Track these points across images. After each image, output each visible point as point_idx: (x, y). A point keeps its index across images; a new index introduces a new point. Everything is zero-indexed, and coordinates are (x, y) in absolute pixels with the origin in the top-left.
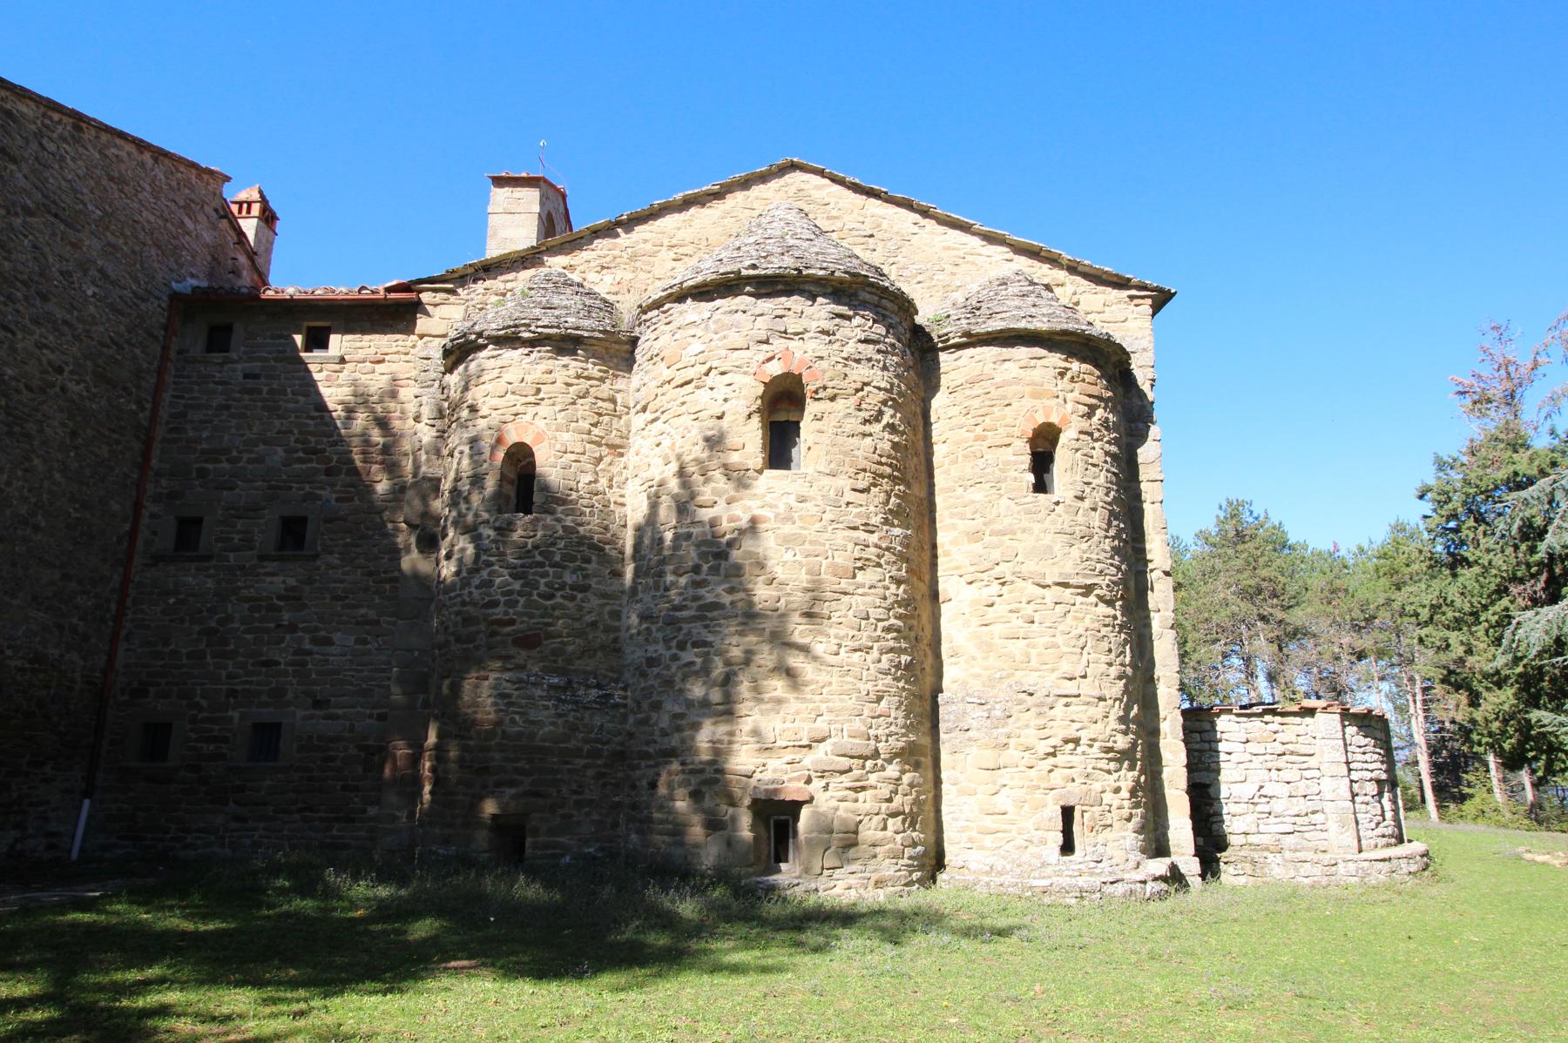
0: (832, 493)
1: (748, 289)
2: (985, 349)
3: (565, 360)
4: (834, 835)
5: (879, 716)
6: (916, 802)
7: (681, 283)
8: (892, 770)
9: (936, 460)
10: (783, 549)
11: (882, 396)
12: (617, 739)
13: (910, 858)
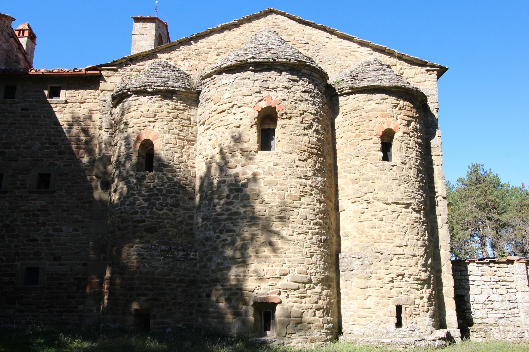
0: (290, 161)
1: (251, 68)
2: (360, 95)
3: (168, 101)
4: (291, 318)
5: (312, 264)
6: (329, 303)
7: (220, 66)
8: (318, 289)
9: (338, 146)
10: (267, 187)
11: (312, 117)
12: (192, 274)
13: (326, 329)
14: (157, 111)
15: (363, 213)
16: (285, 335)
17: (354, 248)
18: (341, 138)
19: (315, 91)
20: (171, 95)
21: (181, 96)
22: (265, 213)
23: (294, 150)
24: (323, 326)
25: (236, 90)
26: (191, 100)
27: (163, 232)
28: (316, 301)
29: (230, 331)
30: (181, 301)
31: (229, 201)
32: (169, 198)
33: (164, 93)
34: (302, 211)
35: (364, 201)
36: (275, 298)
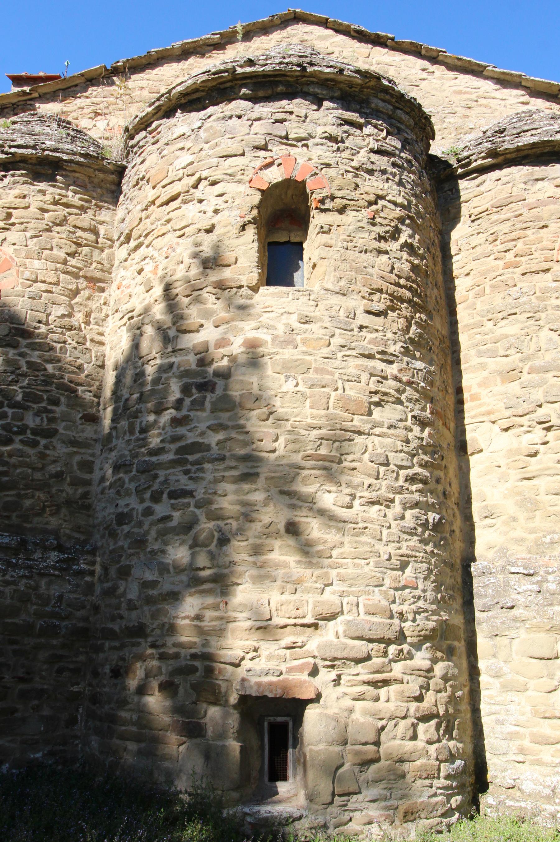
0: (342, 313)
1: (244, 91)
2: (514, 169)
3: (43, 186)
4: (349, 747)
6: (452, 700)
7: (169, 92)
9: (458, 296)
10: (282, 377)
11: (398, 212)
12: (80, 613)
13: (447, 777)
14: (13, 206)
15: (535, 455)
16: (329, 799)
17: (513, 548)
18: (468, 274)
19: (402, 155)
20: (50, 172)
21: (77, 175)
22: (276, 444)
23: (353, 287)
24: (439, 770)
25: (206, 146)
26: (101, 188)
27: (9, 499)
28: (417, 693)
29: (170, 782)
30: (46, 687)
31: (179, 415)
32: (31, 413)
33: (35, 165)
34: (376, 442)
35: (534, 423)
36: (301, 684)
